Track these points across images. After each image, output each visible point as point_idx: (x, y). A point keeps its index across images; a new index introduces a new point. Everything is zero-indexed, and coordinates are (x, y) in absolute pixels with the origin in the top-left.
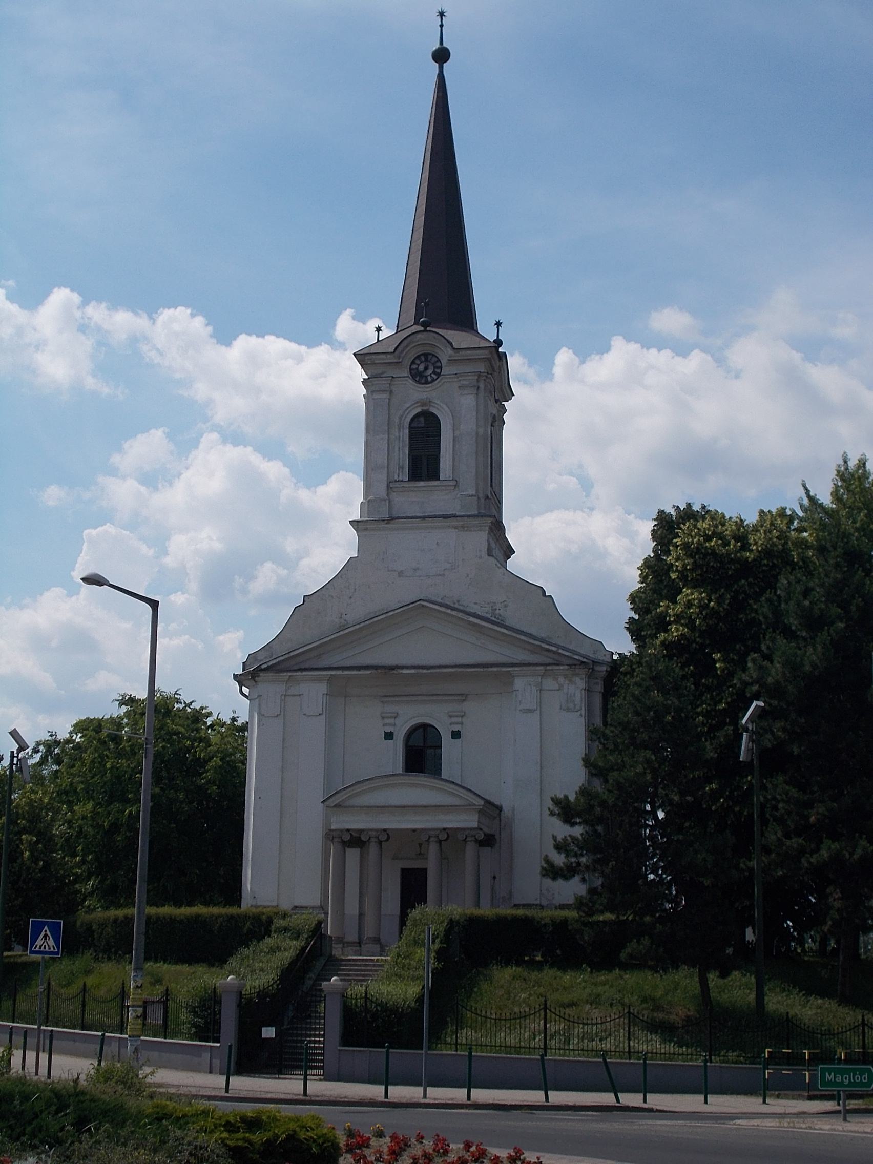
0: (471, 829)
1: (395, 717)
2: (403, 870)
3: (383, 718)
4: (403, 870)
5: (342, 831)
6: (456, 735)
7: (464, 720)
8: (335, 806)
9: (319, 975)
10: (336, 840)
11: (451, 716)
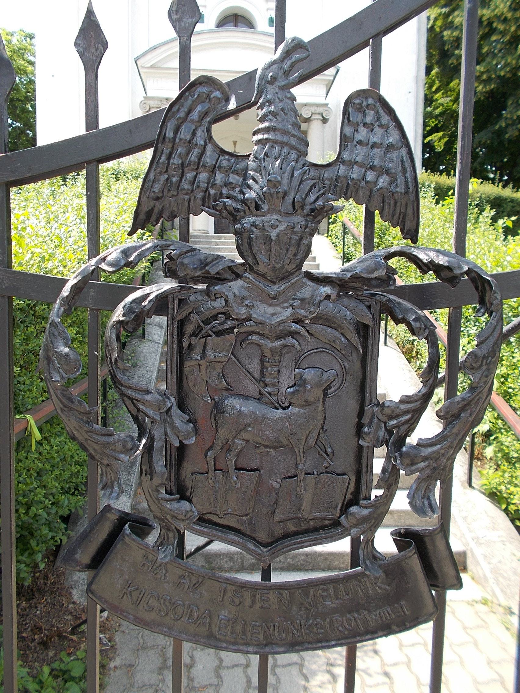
0: (318, 105)
8: (152, 67)
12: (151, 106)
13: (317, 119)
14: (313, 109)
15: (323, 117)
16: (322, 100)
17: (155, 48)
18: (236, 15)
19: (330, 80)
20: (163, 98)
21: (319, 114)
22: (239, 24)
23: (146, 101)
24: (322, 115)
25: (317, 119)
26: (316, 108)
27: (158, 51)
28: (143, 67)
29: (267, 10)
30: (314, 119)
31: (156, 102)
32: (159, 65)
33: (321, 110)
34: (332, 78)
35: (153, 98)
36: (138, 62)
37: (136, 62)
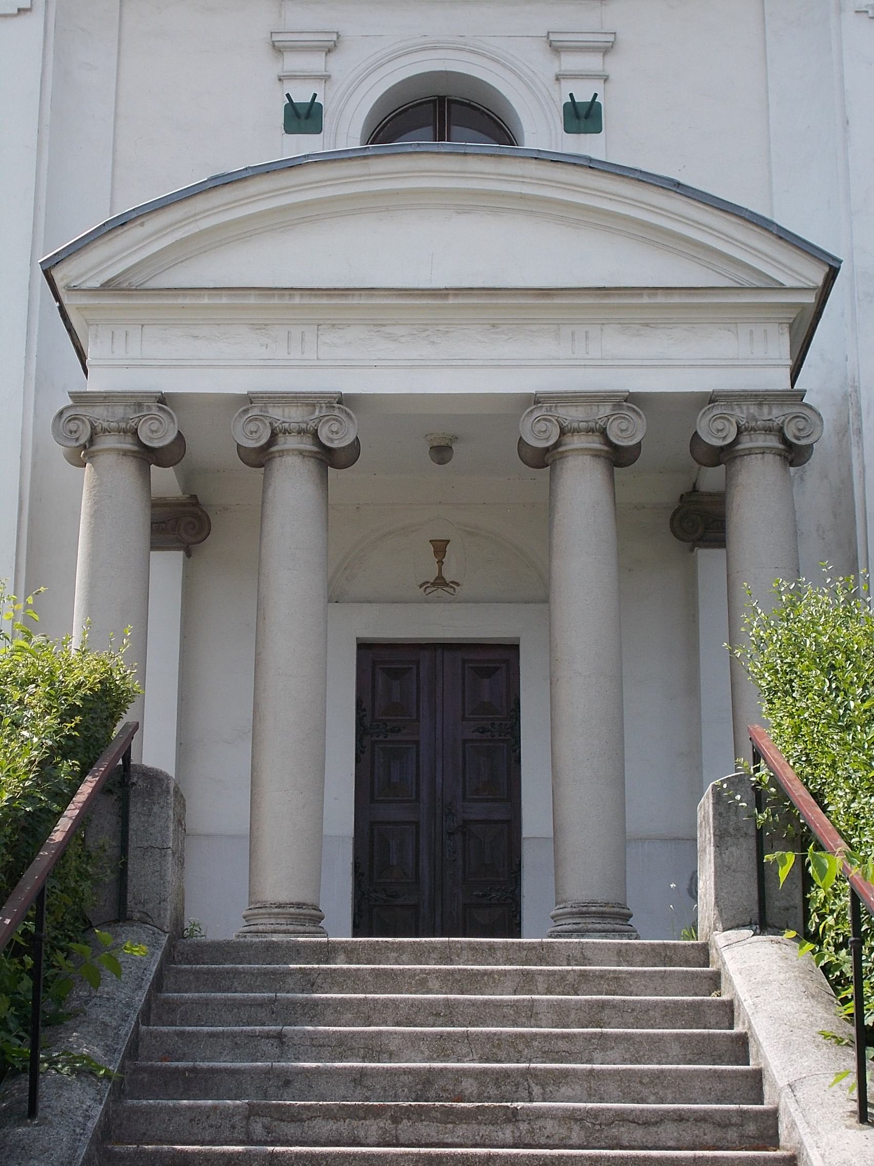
0: (761, 398)
1: (329, 51)
2: (364, 647)
3: (278, 49)
4: (364, 647)
6: (583, 117)
7: (614, 66)
8: (108, 287)
9: (133, 1049)
10: (108, 442)
11: (556, 49)
12: (101, 424)
13: (763, 451)
14: (742, 414)
15: (784, 440)
16: (779, 380)
17: (122, 223)
18: (441, 99)
19: (803, 306)
20: (148, 395)
21: (768, 430)
22: (455, 129)
23: (80, 411)
24: (780, 432)
25: (763, 451)
26: (753, 410)
27: (134, 233)
28: (71, 289)
29: (557, 79)
30: (750, 452)
31: (120, 411)
32: (136, 281)
33: (776, 414)
34: (810, 299)
35: (106, 398)
36: (57, 275)
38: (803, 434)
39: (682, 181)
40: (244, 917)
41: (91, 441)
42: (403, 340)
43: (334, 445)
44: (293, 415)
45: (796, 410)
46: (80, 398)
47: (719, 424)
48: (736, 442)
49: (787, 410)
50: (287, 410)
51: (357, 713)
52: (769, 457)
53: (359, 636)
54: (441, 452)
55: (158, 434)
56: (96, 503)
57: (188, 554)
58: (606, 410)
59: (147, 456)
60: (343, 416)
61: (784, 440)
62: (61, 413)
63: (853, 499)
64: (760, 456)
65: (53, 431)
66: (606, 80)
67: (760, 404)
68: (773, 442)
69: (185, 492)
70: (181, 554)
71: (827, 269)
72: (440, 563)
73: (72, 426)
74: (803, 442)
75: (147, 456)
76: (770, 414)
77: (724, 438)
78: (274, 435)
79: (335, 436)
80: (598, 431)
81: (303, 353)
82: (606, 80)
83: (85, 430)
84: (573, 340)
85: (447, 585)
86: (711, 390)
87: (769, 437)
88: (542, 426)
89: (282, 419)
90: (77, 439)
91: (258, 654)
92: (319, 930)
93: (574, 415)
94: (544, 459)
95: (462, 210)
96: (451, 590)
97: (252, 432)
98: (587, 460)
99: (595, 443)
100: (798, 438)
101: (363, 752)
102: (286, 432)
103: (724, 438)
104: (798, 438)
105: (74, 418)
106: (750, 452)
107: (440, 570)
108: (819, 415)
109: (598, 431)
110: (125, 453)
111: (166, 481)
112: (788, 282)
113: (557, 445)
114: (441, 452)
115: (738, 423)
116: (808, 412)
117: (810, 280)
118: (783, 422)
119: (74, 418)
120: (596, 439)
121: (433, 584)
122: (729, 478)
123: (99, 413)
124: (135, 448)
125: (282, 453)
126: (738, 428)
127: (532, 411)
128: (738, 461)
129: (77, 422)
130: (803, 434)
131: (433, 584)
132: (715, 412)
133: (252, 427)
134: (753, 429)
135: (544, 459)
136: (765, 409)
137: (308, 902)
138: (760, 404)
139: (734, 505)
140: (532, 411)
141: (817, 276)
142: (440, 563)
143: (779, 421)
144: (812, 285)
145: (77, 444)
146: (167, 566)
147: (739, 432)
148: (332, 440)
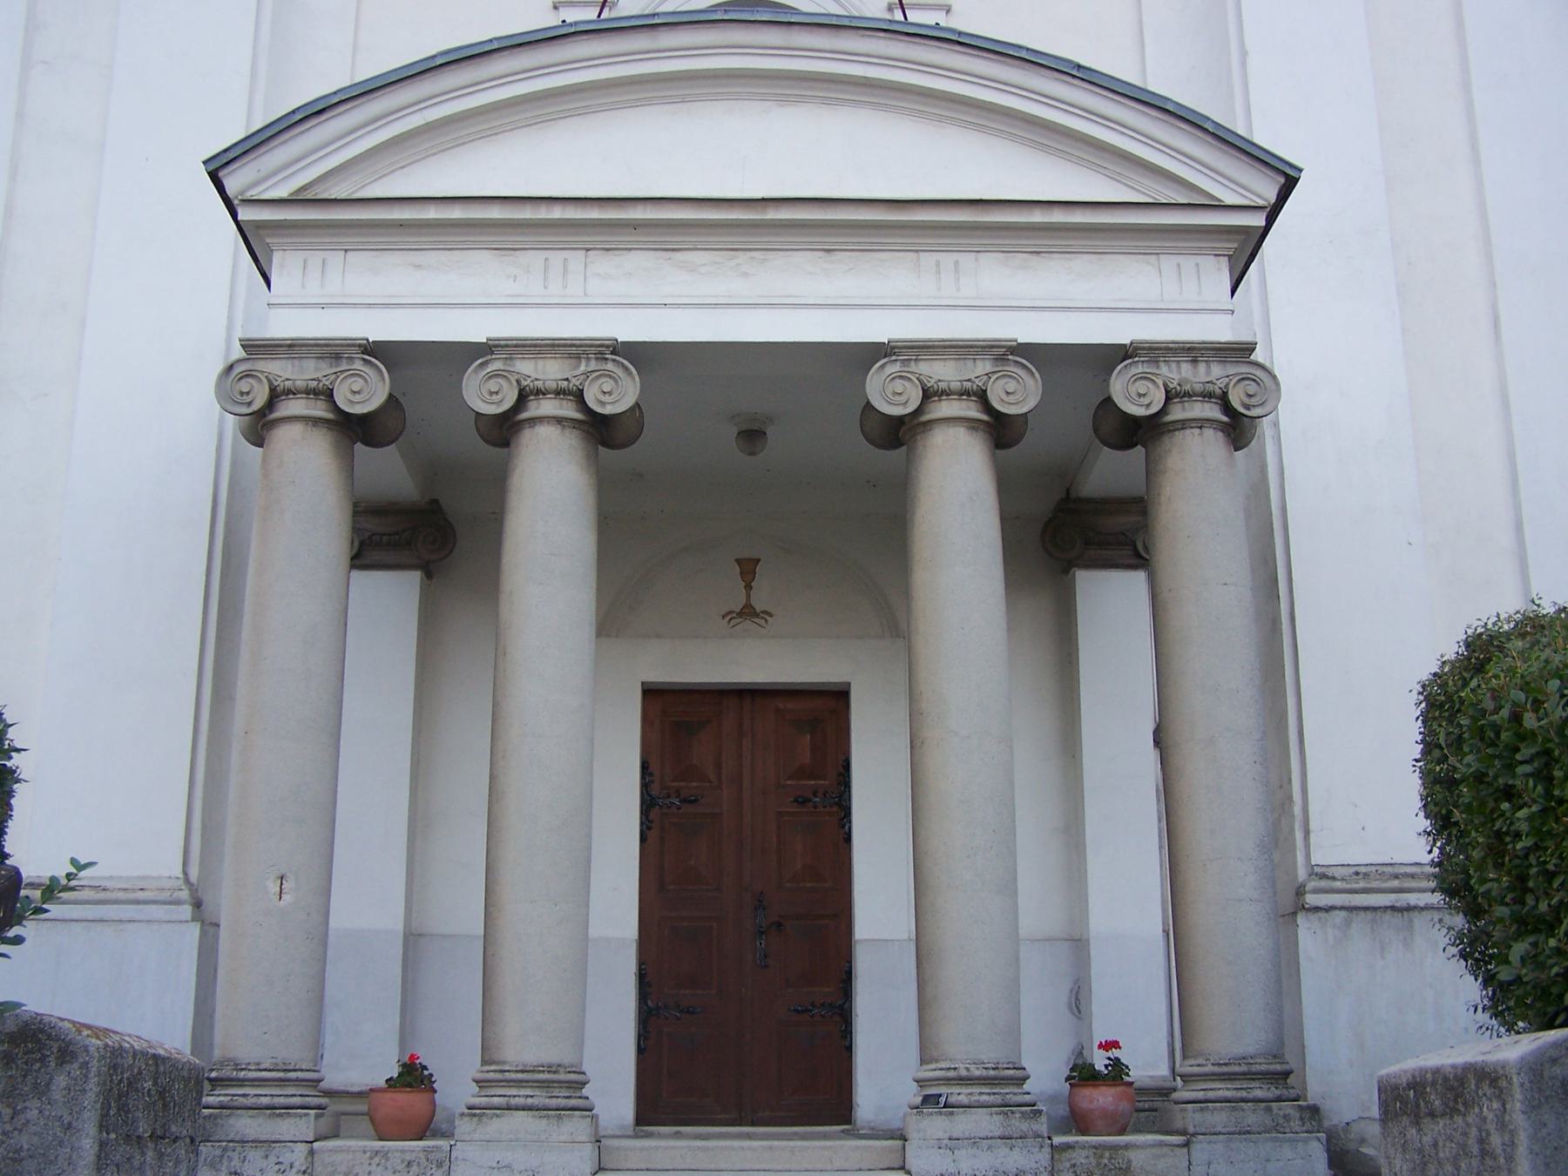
2: (652, 694)
4: (652, 694)
5: (332, 351)
13: (1201, 423)
15: (1227, 408)
20: (350, 344)
21: (1207, 396)
24: (982, 397)
26: (1186, 370)
30: (1184, 424)
33: (1214, 374)
35: (291, 348)
36: (232, 184)
37: (215, 177)
38: (1253, 401)
39: (1082, 63)
40: (477, 1082)
41: (271, 404)
42: (702, 270)
43: (608, 410)
44: (550, 371)
45: (1244, 369)
46: (255, 348)
47: (1142, 386)
48: (1163, 411)
49: (1232, 369)
50: (541, 362)
51: (643, 778)
52: (1209, 433)
53: (646, 679)
54: (752, 436)
55: (365, 392)
56: (310, 478)
57: (428, 575)
58: (983, 367)
59: (354, 430)
60: (619, 372)
61: (1227, 408)
62: (231, 367)
63: (1270, 507)
64: (1197, 431)
65: (1423, 1071)
66: (948, 12)
67: (1195, 361)
68: (1212, 411)
69: (412, 481)
70: (416, 576)
71: (1282, 180)
72: (749, 587)
73: (244, 386)
74: (1254, 412)
75: (354, 430)
76: (1208, 373)
77: (1148, 406)
78: (523, 397)
79: (606, 399)
80: (975, 394)
81: (565, 287)
82: (948, 12)
83: (264, 394)
84: (939, 272)
85: (757, 615)
86: (1127, 342)
87: (1207, 406)
88: (899, 386)
89: (534, 376)
90: (250, 404)
91: (495, 705)
92: (580, 1103)
93: (943, 372)
94: (899, 434)
95: (784, 100)
96: (762, 622)
97: (491, 393)
98: (960, 434)
99: (972, 410)
100: (1247, 407)
101: (649, 828)
102: (539, 393)
103: (1148, 406)
104: (1247, 407)
105: (247, 375)
106: (1184, 424)
107: (748, 597)
108: (1275, 377)
109: (975, 394)
110: (315, 421)
111: (389, 471)
112: (1230, 199)
113: (918, 411)
114: (752, 436)
115: (1165, 385)
116: (1259, 373)
117: (1259, 196)
118: (1227, 385)
119: (247, 375)
120: (972, 405)
121: (740, 614)
122: (1151, 471)
123: (282, 370)
124: (330, 416)
125: (534, 421)
126: (1167, 392)
127: (883, 366)
128: (1166, 439)
129: (250, 380)
130: (1253, 401)
131: (740, 614)
132: (1134, 370)
133: (493, 385)
134: (1188, 394)
135: (899, 434)
136: (1202, 367)
137: (566, 1061)
138: (1195, 361)
139: (1163, 499)
140: (883, 366)
141: (1268, 191)
142: (749, 587)
143: (1221, 384)
144: (1261, 203)
145: (249, 411)
146: (391, 596)
147: (1168, 399)
148: (603, 404)
